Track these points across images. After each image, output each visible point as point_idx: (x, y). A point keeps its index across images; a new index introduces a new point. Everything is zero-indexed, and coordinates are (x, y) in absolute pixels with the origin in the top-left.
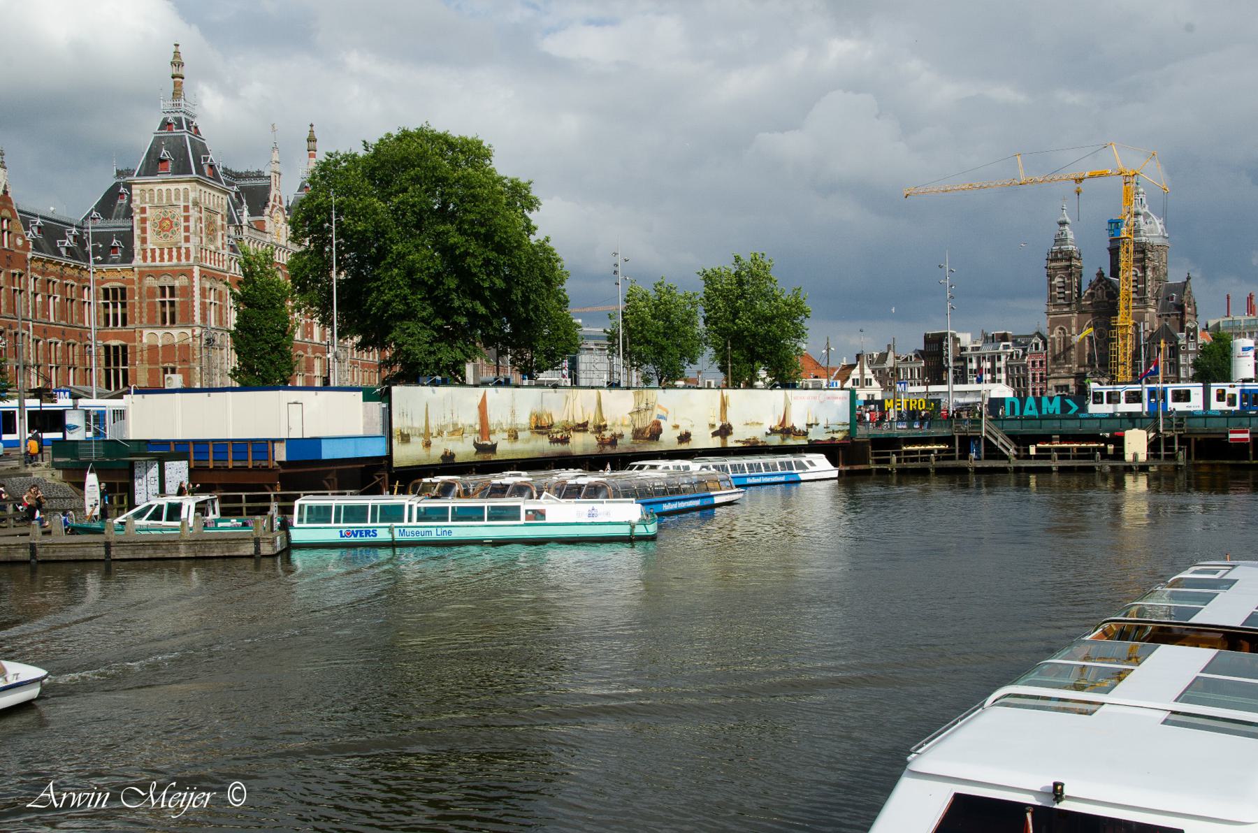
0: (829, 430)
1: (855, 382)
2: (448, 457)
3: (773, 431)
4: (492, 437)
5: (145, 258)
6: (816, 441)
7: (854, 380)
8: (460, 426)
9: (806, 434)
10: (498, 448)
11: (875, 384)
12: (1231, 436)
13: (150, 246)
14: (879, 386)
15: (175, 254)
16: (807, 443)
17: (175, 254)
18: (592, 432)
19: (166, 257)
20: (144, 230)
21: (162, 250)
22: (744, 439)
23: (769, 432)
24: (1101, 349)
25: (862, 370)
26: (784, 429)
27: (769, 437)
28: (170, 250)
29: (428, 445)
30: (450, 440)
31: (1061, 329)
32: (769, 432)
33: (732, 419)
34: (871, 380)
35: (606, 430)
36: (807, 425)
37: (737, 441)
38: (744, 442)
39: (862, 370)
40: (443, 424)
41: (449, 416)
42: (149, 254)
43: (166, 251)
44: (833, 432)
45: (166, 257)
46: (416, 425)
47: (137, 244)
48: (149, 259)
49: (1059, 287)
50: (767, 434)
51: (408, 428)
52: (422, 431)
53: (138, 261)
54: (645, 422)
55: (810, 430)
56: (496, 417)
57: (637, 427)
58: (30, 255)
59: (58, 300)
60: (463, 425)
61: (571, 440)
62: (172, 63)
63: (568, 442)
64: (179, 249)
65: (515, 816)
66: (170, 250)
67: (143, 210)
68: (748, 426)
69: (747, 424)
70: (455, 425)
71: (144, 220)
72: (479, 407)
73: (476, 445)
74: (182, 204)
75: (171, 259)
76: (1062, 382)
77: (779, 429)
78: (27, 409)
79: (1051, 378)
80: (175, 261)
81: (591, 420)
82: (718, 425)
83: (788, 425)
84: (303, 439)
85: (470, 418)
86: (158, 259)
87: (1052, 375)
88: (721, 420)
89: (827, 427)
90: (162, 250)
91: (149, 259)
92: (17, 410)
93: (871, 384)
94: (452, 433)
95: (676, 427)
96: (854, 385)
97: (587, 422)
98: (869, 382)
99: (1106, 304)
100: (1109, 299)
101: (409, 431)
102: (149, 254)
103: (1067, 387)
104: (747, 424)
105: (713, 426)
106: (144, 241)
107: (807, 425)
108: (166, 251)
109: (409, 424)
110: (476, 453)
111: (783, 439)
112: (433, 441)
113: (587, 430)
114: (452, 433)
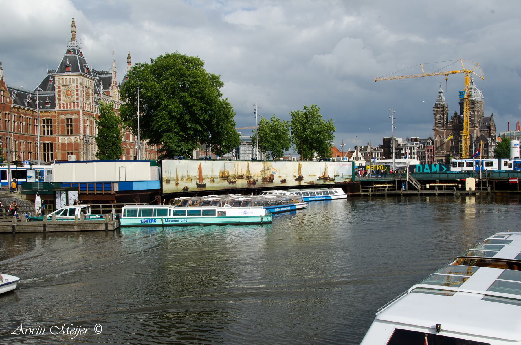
0: (343, 178)
1: (354, 158)
2: (186, 189)
3: (320, 178)
4: (204, 181)
5: (60, 107)
6: (338, 182)
7: (353, 157)
8: (190, 176)
9: (334, 180)
10: (206, 186)
11: (363, 159)
12: (510, 181)
13: (62, 102)
14: (364, 160)
15: (72, 105)
16: (334, 183)
17: (72, 105)
18: (245, 179)
19: (69, 106)
20: (60, 95)
21: (67, 103)
22: (308, 182)
23: (318, 179)
24: (456, 144)
25: (357, 153)
26: (324, 178)
27: (319, 181)
28: (71, 104)
29: (177, 184)
30: (187, 182)
31: (439, 136)
32: (318, 179)
33: (303, 174)
34: (361, 157)
35: (251, 178)
36: (334, 176)
37: (305, 183)
38: (308, 183)
39: (357, 153)
40: (183, 175)
41: (186, 172)
42: (62, 105)
43: (69, 104)
44: (345, 179)
45: (69, 106)
46: (172, 176)
47: (57, 101)
48: (62, 107)
49: (439, 119)
50: (318, 180)
51: (169, 177)
52: (175, 179)
53: (57, 108)
54: (267, 175)
55: (335, 178)
56: (205, 173)
57: (264, 177)
58: (12, 106)
59: (24, 124)
60: (192, 176)
61: (236, 182)
62: (71, 26)
63: (235, 183)
64: (74, 103)
65: (213, 338)
66: (71, 104)
67: (59, 87)
68: (310, 177)
69: (309, 176)
70: (188, 176)
71: (59, 91)
72: (198, 169)
73: (197, 184)
74: (75, 85)
75: (71, 107)
76: (440, 158)
77: (323, 177)
78: (11, 170)
79: (435, 157)
80: (72, 108)
81: (245, 174)
82: (297, 176)
83: (326, 176)
84: (125, 182)
85: (194, 173)
86: (65, 107)
87: (436, 156)
88: (299, 174)
89: (343, 177)
90: (67, 103)
91: (62, 107)
92: (7, 170)
93: (361, 159)
94: (187, 180)
95: (280, 177)
96: (354, 159)
97: (243, 175)
98: (360, 158)
99: (458, 126)
100: (460, 124)
101: (170, 179)
102: (62, 105)
103: (442, 160)
104: (309, 176)
105: (295, 176)
106: (60, 100)
107: (334, 176)
108: (69, 104)
109: (170, 176)
110: (197, 188)
111: (324, 182)
112: (179, 182)
113: (243, 178)
114: (187, 180)
